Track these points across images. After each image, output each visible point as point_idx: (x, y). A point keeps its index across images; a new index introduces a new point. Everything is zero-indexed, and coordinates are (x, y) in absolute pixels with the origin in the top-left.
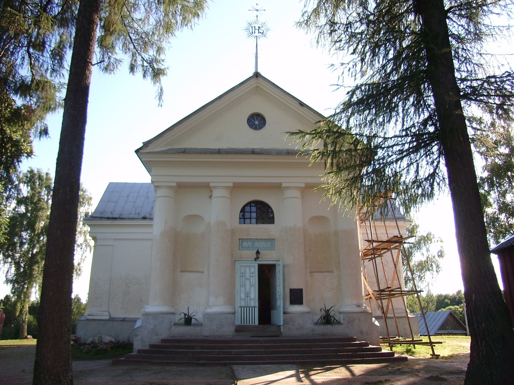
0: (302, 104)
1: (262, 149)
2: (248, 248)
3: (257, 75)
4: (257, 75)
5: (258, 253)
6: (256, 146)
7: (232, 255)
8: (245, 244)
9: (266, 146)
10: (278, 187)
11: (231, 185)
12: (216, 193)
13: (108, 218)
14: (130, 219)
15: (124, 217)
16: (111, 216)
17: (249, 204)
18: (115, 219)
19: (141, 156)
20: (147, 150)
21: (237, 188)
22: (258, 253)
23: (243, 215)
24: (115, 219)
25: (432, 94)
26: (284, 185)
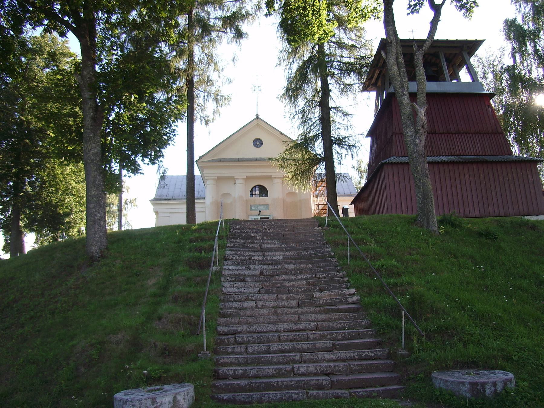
0: (281, 133)
1: (261, 158)
2: (255, 210)
3: (257, 117)
4: (257, 117)
5: (260, 211)
6: (258, 156)
7: (247, 213)
8: (253, 208)
9: (263, 156)
10: (270, 178)
11: (246, 177)
12: (238, 182)
13: (165, 199)
14: (179, 199)
15: (175, 198)
16: (167, 198)
17: (255, 187)
18: (170, 199)
19: (198, 164)
20: (202, 160)
21: (248, 179)
22: (260, 211)
23: (252, 193)
24: (170, 199)
25: (526, 27)
26: (272, 177)
